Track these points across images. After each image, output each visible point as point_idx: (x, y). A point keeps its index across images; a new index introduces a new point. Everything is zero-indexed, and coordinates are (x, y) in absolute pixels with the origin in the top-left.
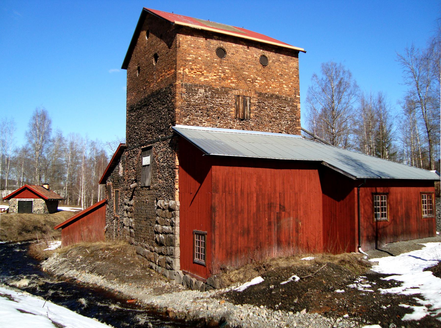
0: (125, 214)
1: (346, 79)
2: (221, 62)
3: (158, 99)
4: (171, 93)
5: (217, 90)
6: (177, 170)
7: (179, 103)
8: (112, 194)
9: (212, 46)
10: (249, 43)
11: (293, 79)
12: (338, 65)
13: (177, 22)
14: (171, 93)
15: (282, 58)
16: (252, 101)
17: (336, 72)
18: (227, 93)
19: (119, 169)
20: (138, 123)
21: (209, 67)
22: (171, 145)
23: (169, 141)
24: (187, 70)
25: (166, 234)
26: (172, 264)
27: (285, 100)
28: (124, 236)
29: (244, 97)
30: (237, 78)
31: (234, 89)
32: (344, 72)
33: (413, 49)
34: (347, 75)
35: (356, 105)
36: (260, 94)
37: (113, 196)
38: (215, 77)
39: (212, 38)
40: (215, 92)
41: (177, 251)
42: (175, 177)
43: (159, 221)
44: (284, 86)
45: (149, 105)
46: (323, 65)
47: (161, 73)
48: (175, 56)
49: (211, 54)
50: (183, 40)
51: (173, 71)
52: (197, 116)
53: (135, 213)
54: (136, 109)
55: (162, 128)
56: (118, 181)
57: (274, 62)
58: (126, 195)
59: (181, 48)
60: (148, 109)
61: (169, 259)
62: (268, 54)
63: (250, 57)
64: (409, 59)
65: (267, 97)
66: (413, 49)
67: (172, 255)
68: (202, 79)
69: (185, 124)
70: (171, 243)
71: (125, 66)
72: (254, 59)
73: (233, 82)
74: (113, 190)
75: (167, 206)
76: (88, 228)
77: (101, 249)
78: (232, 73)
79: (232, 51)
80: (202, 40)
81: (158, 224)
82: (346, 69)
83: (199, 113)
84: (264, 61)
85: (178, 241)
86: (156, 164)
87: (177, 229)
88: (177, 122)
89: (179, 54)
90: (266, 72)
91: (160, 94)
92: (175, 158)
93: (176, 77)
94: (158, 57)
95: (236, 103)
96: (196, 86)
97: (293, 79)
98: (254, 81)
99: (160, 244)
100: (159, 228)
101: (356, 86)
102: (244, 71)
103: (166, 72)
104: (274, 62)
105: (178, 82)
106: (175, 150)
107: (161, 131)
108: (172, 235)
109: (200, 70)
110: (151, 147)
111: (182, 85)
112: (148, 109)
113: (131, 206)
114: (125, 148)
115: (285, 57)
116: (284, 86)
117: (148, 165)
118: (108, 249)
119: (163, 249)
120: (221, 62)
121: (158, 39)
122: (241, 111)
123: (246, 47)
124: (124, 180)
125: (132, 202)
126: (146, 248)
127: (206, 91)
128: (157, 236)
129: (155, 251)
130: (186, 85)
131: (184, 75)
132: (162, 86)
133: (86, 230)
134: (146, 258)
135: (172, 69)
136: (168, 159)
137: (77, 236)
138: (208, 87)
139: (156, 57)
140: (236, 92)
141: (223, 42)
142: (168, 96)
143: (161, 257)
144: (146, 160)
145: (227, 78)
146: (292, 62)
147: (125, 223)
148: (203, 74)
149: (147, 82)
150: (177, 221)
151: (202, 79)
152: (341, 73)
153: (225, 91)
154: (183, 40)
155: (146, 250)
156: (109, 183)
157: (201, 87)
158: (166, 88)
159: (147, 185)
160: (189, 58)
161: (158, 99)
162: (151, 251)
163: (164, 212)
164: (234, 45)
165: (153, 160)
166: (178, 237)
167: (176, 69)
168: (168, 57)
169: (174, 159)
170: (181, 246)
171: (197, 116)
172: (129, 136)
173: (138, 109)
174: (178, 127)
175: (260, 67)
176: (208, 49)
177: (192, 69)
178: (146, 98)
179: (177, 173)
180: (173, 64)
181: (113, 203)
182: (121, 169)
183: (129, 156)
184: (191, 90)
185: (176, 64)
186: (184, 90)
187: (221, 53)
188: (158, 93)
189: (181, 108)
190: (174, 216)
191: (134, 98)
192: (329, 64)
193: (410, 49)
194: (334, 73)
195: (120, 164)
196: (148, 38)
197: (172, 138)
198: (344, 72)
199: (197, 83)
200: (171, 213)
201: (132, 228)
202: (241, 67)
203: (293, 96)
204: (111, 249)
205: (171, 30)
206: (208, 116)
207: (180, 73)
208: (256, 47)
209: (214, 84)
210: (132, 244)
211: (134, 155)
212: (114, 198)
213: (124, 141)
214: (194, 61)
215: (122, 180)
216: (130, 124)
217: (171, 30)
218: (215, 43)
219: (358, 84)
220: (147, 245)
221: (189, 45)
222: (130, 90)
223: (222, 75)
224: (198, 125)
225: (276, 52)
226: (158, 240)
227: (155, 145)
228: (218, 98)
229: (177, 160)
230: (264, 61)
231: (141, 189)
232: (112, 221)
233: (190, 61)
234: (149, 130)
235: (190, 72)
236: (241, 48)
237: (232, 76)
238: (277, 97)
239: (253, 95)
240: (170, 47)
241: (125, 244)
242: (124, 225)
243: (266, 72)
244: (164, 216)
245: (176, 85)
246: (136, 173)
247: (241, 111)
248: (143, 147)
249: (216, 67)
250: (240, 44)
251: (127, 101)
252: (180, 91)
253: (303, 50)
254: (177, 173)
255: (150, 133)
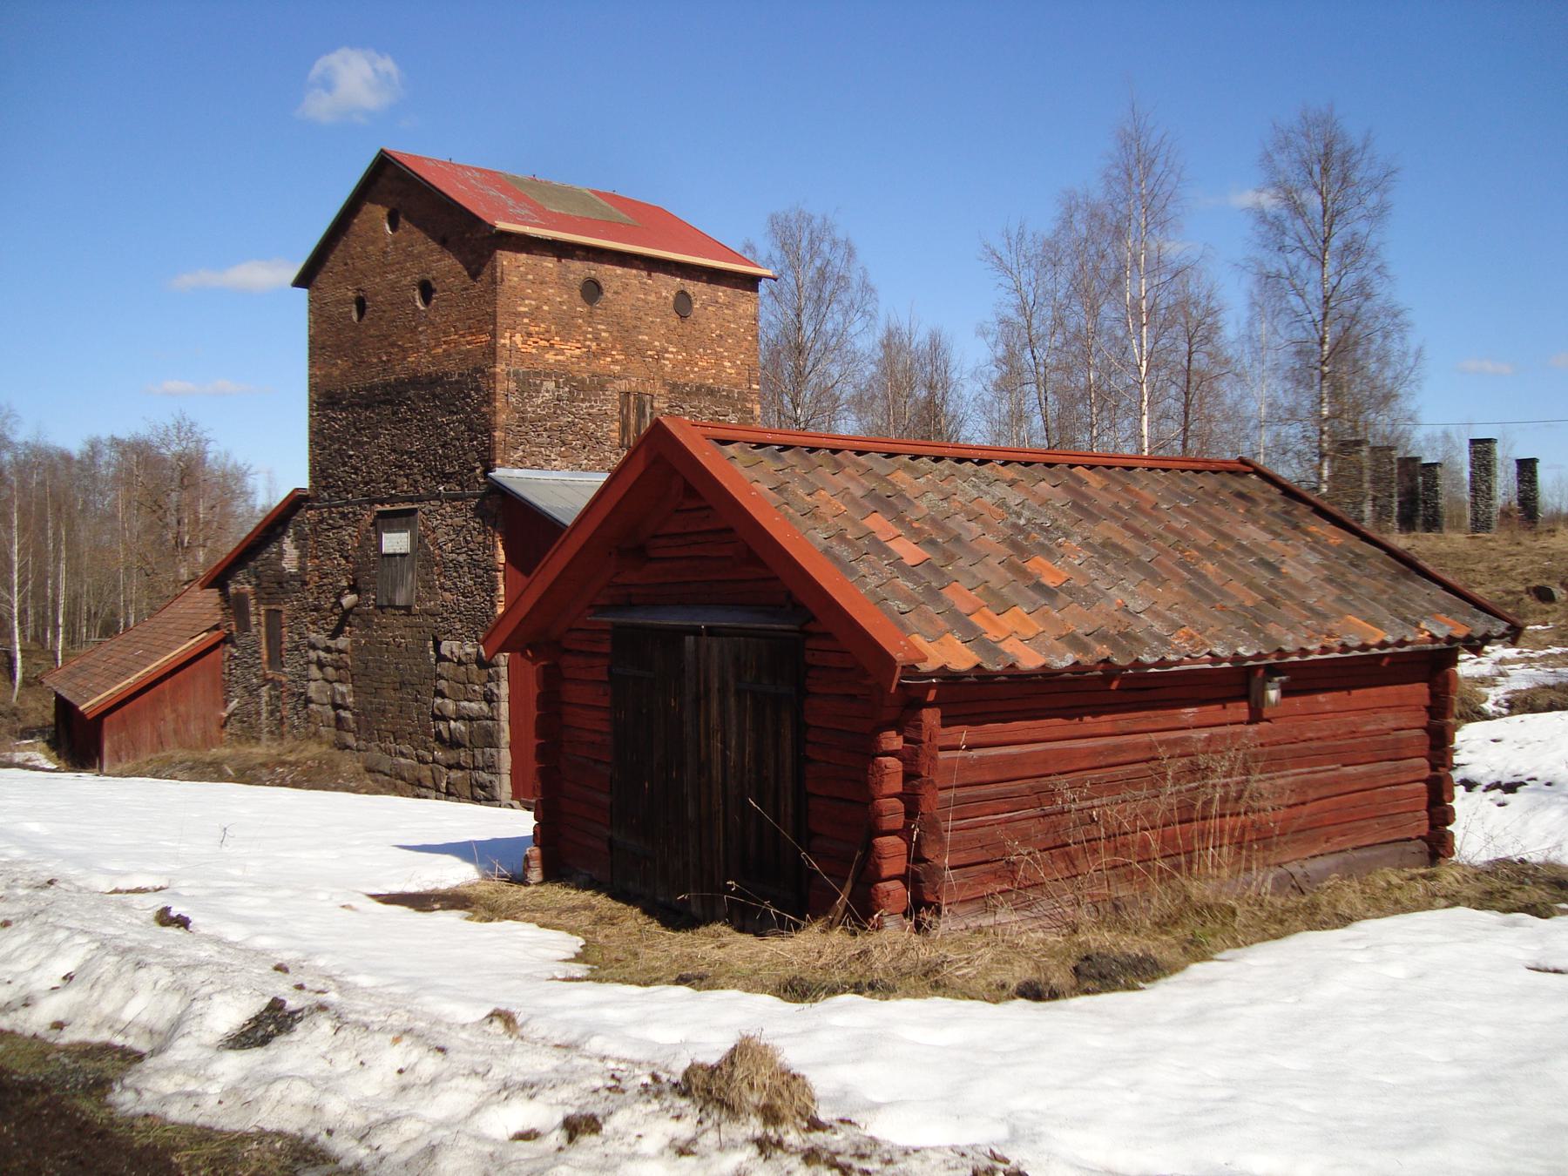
0: (314, 671)
1: (838, 263)
2: (591, 314)
3: (435, 396)
4: (478, 390)
5: (583, 381)
6: (500, 575)
7: (502, 418)
8: (253, 620)
9: (572, 277)
10: (653, 265)
11: (745, 344)
12: (817, 223)
13: (502, 225)
14: (478, 390)
15: (723, 293)
16: (656, 405)
17: (812, 242)
18: (603, 388)
19: (281, 554)
20: (360, 444)
21: (566, 327)
22: (479, 511)
23: (473, 503)
24: (518, 338)
25: (471, 719)
26: (493, 787)
27: (727, 396)
28: (313, 728)
29: (639, 397)
30: (624, 351)
31: (619, 378)
32: (834, 244)
33: (1021, 236)
34: (841, 252)
35: (865, 341)
36: (674, 387)
37: (259, 624)
38: (578, 352)
39: (571, 256)
40: (581, 387)
41: (505, 758)
42: (494, 589)
43: (447, 692)
44: (727, 364)
45: (399, 404)
46: (773, 220)
47: (446, 334)
48: (493, 303)
49: (571, 296)
50: (509, 262)
51: (485, 338)
52: (540, 445)
53: (361, 674)
54: (352, 405)
55: (448, 469)
56: (277, 586)
57: (704, 307)
58: (313, 623)
59: (506, 283)
60: (394, 413)
61: (484, 777)
62: (692, 287)
63: (652, 298)
64: (1009, 259)
65: (688, 394)
66: (1021, 236)
67: (492, 767)
68: (550, 357)
69: (515, 465)
70: (490, 739)
71: (305, 279)
72: (662, 301)
73: (615, 362)
74: (257, 615)
75: (473, 657)
76: (175, 711)
77: (264, 765)
78: (615, 339)
79: (616, 285)
80: (549, 263)
81: (443, 696)
82: (840, 235)
83: (544, 439)
84: (683, 304)
85: (505, 737)
86: (429, 553)
87: (504, 708)
88: (498, 462)
89: (501, 300)
90: (687, 332)
91: (442, 385)
92: (495, 546)
93: (494, 353)
94: (434, 291)
95: (621, 412)
96: (537, 374)
97: (745, 344)
98: (661, 353)
99: (453, 743)
100: (450, 706)
101: (867, 288)
102: (640, 333)
103: (463, 336)
104: (704, 307)
105: (500, 368)
106: (494, 527)
107: (446, 477)
108: (490, 723)
109: (547, 336)
110: (413, 512)
111: (508, 373)
112: (394, 413)
113: (340, 651)
114: (306, 498)
115: (729, 291)
116: (727, 364)
117: (403, 555)
118: (283, 764)
119: (463, 756)
120: (591, 314)
121: (434, 245)
122: (632, 428)
123: (644, 273)
124: (305, 583)
125: (343, 642)
126: (403, 755)
127: (558, 386)
128: (442, 726)
129: (434, 761)
130: (516, 374)
131: (513, 348)
132: (449, 366)
133: (170, 717)
134: (403, 779)
135: (481, 331)
136: (471, 546)
137: (146, 732)
138: (562, 375)
139: (427, 290)
140: (623, 385)
141: (596, 265)
142: (469, 396)
143: (455, 774)
144: (395, 542)
145: (605, 353)
146: (745, 304)
147: (312, 693)
148: (552, 346)
149: (393, 345)
150: (504, 690)
151: (550, 357)
152: (825, 247)
153: (599, 384)
154: (509, 262)
155: (402, 760)
156: (242, 585)
157: (548, 375)
158: (461, 375)
159: (400, 599)
160: (522, 309)
161: (435, 396)
162: (422, 760)
163: (463, 669)
164: (619, 270)
165: (418, 542)
166: (505, 725)
167: (494, 336)
168: (470, 299)
169: (489, 548)
170: (512, 747)
171: (540, 445)
172: (322, 471)
173: (359, 405)
174: (500, 473)
175: (674, 321)
176: (563, 284)
177: (530, 335)
178: (389, 384)
179: (501, 580)
180: (487, 322)
181: (259, 643)
182: (289, 555)
183: (321, 522)
184: (527, 383)
185: (495, 324)
186: (512, 385)
187: (592, 290)
188: (434, 381)
189: (507, 430)
190: (494, 678)
191: (342, 374)
192: (793, 216)
193: (1014, 235)
194: (804, 243)
195: (288, 541)
196: (394, 228)
197: (483, 497)
198: (834, 244)
199: (540, 367)
200: (484, 672)
201: (346, 708)
202: (634, 322)
203: (745, 386)
204: (291, 764)
205: (479, 236)
206: (564, 444)
207: (504, 345)
208: (666, 272)
209: (576, 367)
210: (348, 747)
211: (342, 522)
212: (263, 630)
213: (304, 482)
214: (534, 315)
215: (297, 584)
216: (318, 438)
217: (479, 236)
218: (579, 269)
219: (873, 280)
220: (406, 748)
221: (523, 277)
222: (317, 349)
223: (594, 346)
224: (542, 468)
225: (709, 282)
226: (446, 735)
227: (426, 507)
228: (583, 401)
229: (501, 552)
230: (683, 304)
231: (378, 612)
232: (252, 692)
233: (524, 315)
234: (400, 468)
235: (524, 343)
236: (633, 275)
237: (614, 348)
238: (711, 392)
239: (659, 389)
240: (474, 275)
241: (325, 748)
242: (309, 701)
243: (687, 332)
244: (463, 678)
245: (494, 374)
246: (354, 572)
247: (632, 428)
248: (379, 508)
249: (579, 327)
250: (632, 267)
251: (311, 376)
252: (504, 386)
253: (769, 273)
254: (501, 580)
255: (407, 476)
